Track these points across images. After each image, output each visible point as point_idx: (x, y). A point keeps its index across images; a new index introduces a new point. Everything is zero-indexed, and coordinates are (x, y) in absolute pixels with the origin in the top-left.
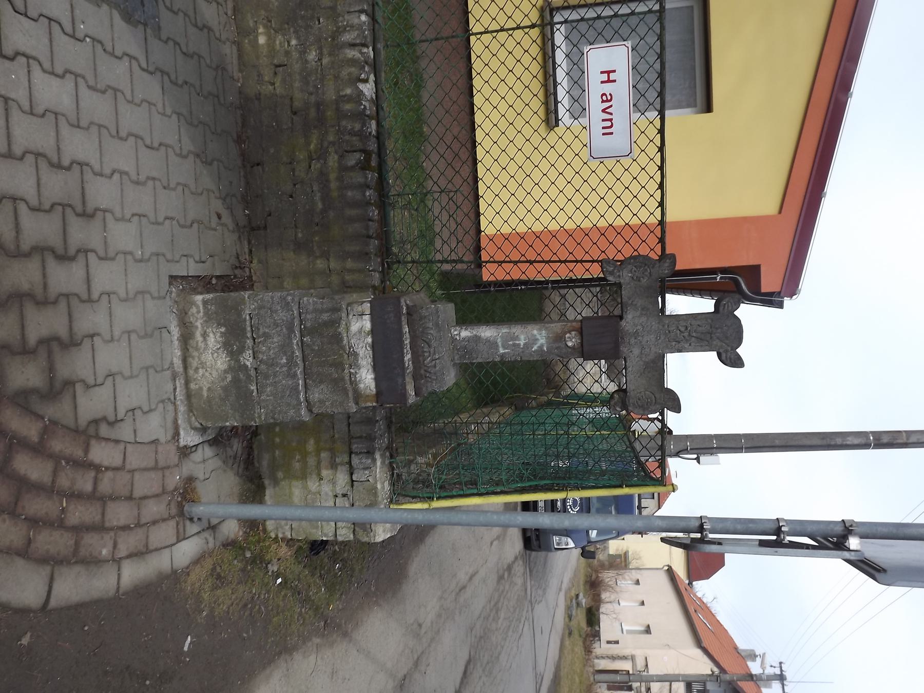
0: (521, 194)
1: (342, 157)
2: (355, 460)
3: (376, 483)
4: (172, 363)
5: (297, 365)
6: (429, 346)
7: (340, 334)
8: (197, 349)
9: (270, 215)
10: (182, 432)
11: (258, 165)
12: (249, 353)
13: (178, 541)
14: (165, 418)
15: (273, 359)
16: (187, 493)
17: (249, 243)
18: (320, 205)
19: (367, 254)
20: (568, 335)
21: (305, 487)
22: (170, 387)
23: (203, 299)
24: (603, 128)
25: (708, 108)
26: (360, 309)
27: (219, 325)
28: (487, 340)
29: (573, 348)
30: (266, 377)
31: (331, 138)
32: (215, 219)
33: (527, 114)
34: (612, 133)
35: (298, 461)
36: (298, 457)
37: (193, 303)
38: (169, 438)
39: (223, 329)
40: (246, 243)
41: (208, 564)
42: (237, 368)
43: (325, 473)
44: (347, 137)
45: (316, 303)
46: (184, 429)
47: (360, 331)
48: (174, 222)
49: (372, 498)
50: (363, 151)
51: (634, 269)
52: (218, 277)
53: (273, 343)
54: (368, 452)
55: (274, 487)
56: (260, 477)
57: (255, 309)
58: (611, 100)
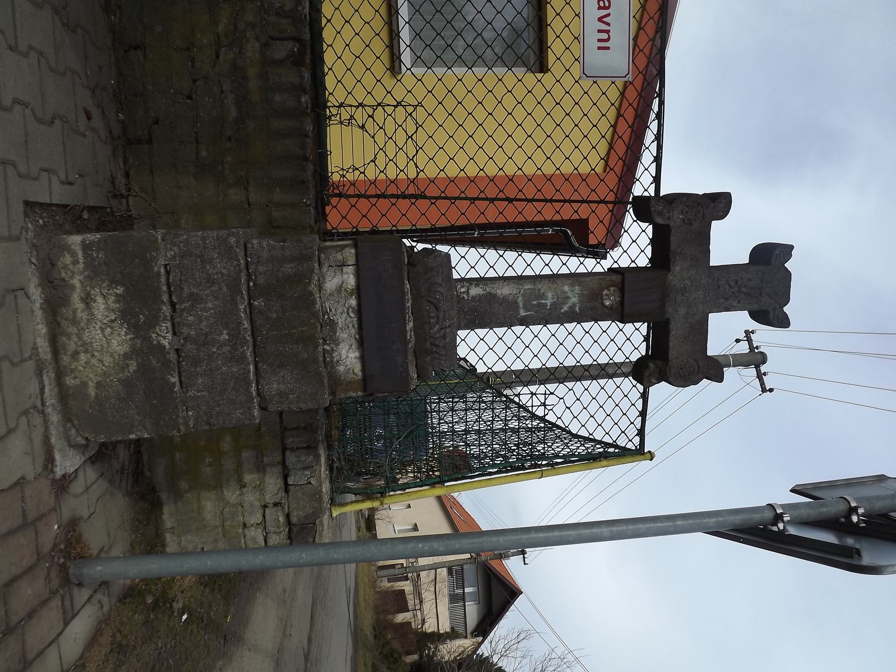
1: (265, 45)
2: (291, 459)
3: (321, 485)
4: (35, 348)
7: (311, 294)
8: (75, 322)
10: (57, 456)
11: (136, 48)
12: (165, 328)
13: (66, 624)
15: (206, 335)
17: (126, 161)
19: (303, 182)
20: (605, 292)
22: (34, 387)
23: (83, 241)
24: (599, 40)
26: (339, 257)
27: (113, 283)
28: (505, 300)
29: (610, 308)
31: (250, 18)
32: (83, 119)
33: (368, 57)
34: (608, 48)
35: (210, 465)
36: (207, 460)
37: (67, 248)
38: (39, 470)
39: (120, 290)
41: (106, 639)
42: (144, 350)
43: (247, 478)
44: (273, 19)
46: (61, 450)
47: (339, 289)
48: (28, 111)
50: (297, 40)
51: (686, 209)
52: (92, 209)
53: (206, 310)
54: (308, 447)
55: (176, 502)
56: (154, 490)
57: (174, 257)
58: (608, 8)
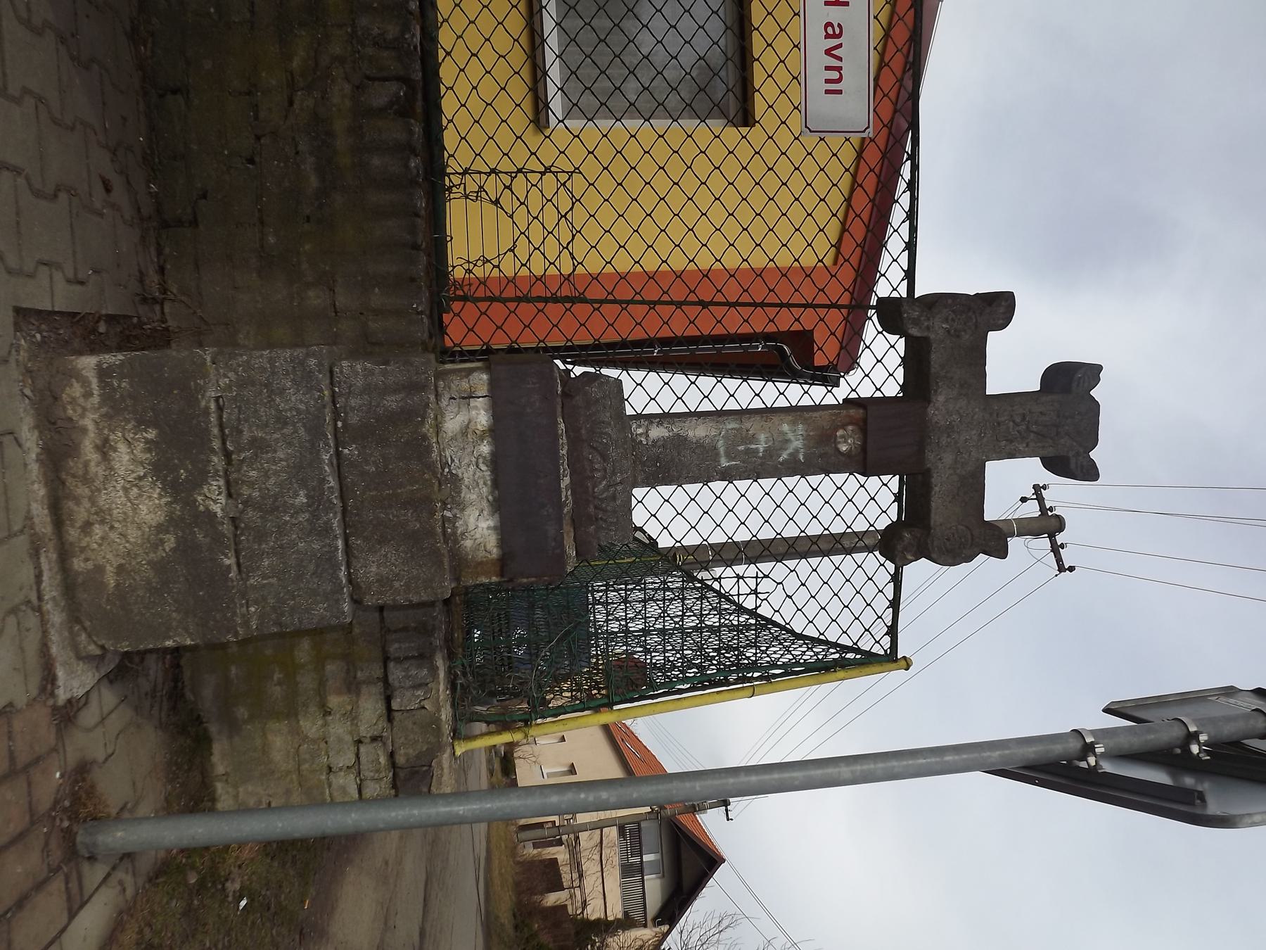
0: (690, 184)
3: (439, 710)
4: (29, 517)
5: (330, 507)
6: (605, 458)
7: (425, 437)
8: (86, 480)
9: (204, 196)
10: (60, 673)
13: (72, 915)
14: (22, 649)
15: (276, 497)
16: (81, 803)
17: (160, 252)
18: (314, 181)
19: (413, 280)
21: (296, 731)
22: (26, 573)
23: (99, 365)
24: (827, 81)
25: (746, 118)
26: (465, 385)
27: (142, 423)
29: (848, 455)
30: (261, 536)
31: (337, 49)
32: (99, 188)
34: (840, 92)
35: (279, 683)
36: (277, 676)
37: (76, 375)
38: (34, 692)
39: (152, 434)
40: (153, 250)
42: (186, 518)
43: (334, 701)
44: (370, 51)
45: (371, 373)
46: (65, 664)
47: (465, 431)
49: (432, 739)
50: (405, 80)
52: (111, 319)
54: (421, 656)
56: (199, 720)
58: (840, 36)
